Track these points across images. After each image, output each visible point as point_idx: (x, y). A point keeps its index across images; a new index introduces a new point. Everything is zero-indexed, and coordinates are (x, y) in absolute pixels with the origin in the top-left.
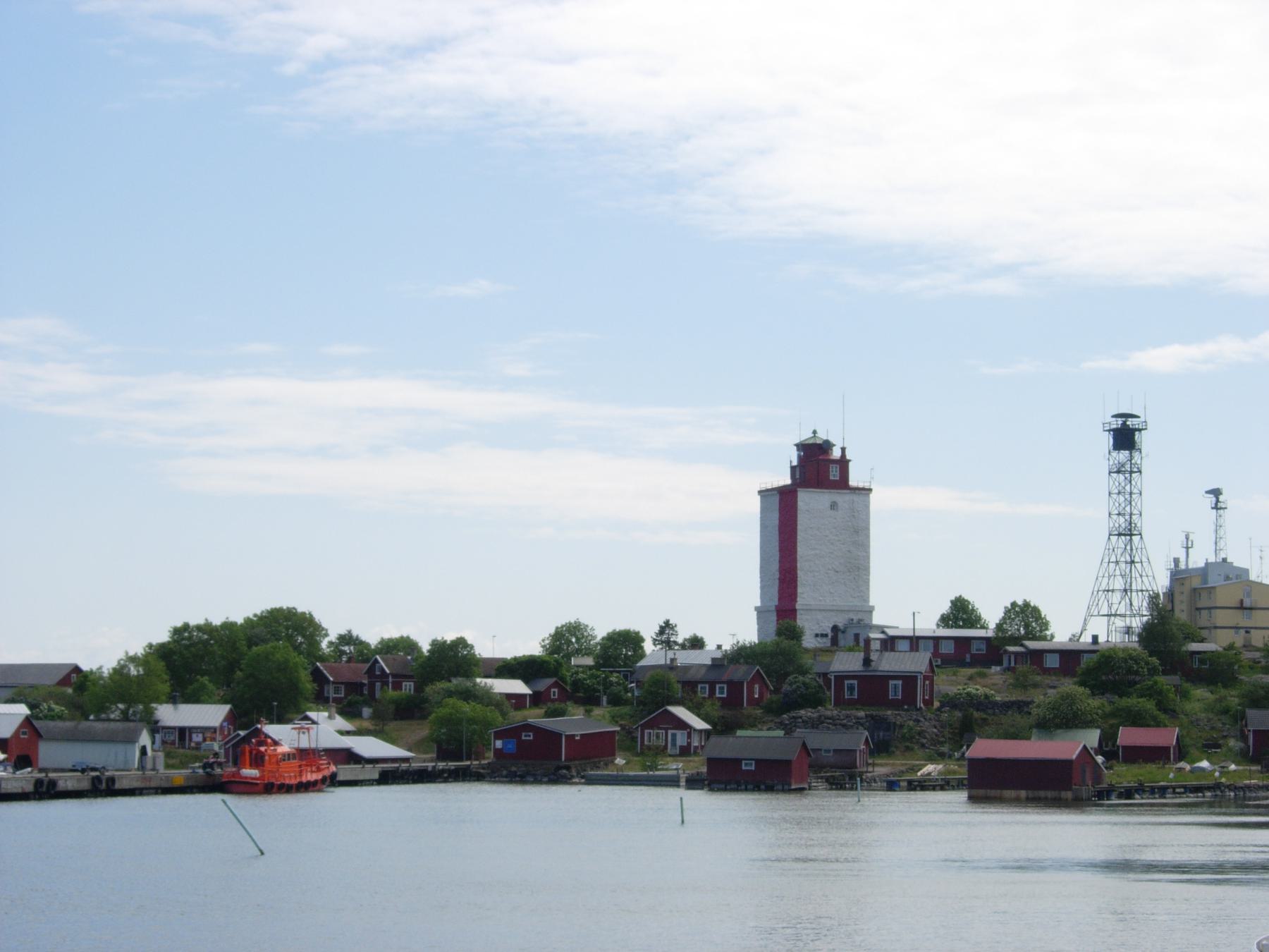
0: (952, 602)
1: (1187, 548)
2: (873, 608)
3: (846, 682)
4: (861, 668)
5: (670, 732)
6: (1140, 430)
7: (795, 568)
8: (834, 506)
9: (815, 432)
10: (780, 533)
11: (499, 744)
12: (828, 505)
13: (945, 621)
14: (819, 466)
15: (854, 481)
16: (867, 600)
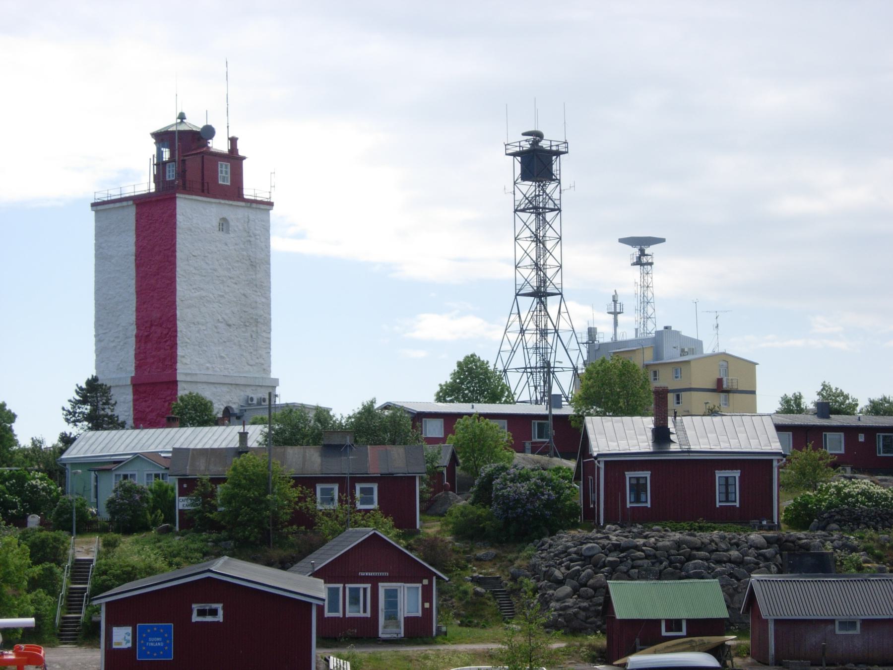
0: (459, 364)
1: (615, 314)
2: (276, 381)
3: (628, 475)
4: (650, 449)
5: (382, 587)
6: (558, 153)
7: (173, 319)
8: (224, 225)
9: (182, 117)
10: (138, 266)
11: (122, 637)
12: (215, 222)
13: (447, 393)
14: (194, 164)
15: (248, 192)
16: (267, 370)
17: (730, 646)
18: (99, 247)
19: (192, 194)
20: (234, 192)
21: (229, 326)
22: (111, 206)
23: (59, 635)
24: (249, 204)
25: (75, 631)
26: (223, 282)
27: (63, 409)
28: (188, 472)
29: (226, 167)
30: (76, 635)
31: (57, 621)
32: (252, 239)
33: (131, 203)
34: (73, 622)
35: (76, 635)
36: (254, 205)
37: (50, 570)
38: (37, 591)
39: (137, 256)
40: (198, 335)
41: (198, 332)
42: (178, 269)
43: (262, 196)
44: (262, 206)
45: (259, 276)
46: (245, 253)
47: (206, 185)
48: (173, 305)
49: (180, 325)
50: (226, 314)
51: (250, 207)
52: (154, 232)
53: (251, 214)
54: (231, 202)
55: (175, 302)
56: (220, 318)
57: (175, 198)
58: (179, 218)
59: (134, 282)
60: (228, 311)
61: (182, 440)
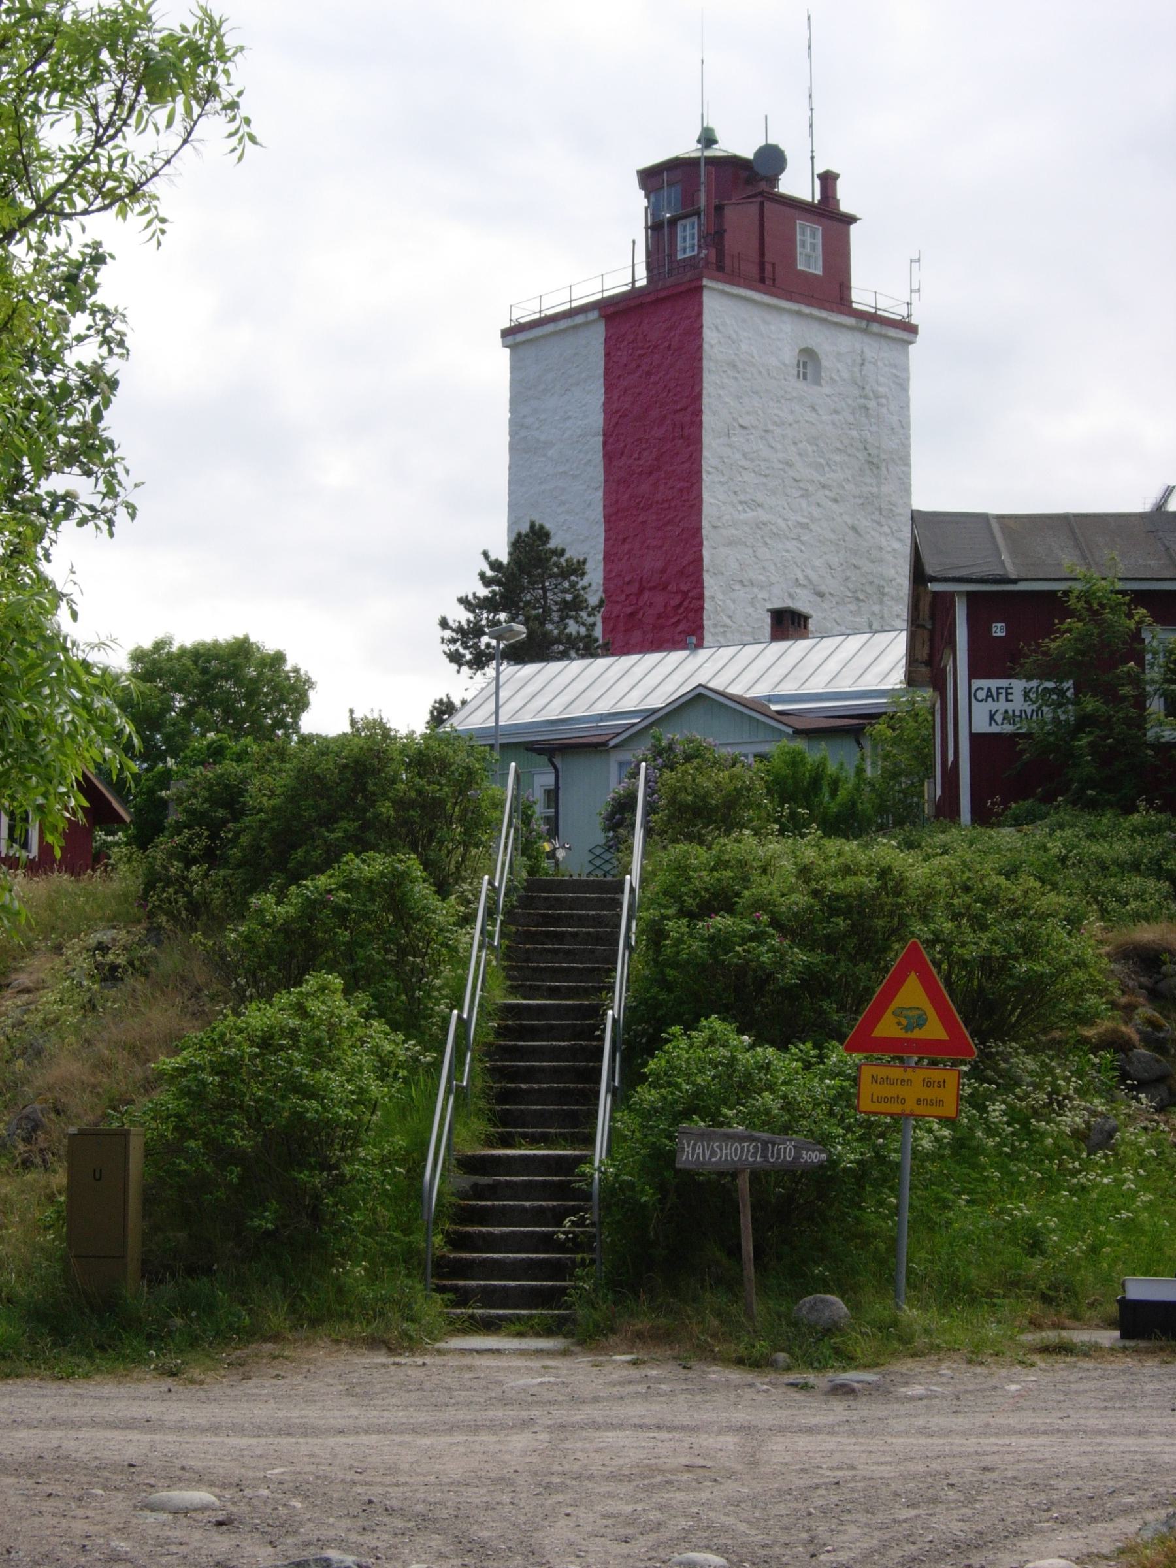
9: (708, 139)
10: (609, 457)
12: (789, 356)
15: (861, 297)
17: (1110, 1324)
18: (517, 426)
19: (739, 285)
20: (830, 291)
21: (821, 595)
22: (550, 328)
23: (445, 1269)
24: (864, 324)
25: (547, 1243)
26: (806, 494)
27: (444, 624)
28: (1012, 573)
29: (814, 236)
30: (557, 1270)
31: (433, 1175)
32: (872, 404)
33: (594, 315)
34: (528, 1191)
35: (557, 1270)
36: (875, 327)
37: (392, 891)
38: (311, 983)
39: (610, 434)
40: (750, 610)
41: (752, 603)
42: (706, 453)
43: (897, 311)
44: (893, 332)
45: (885, 489)
46: (854, 433)
47: (768, 267)
48: (693, 537)
49: (711, 585)
50: (814, 568)
51: (865, 331)
52: (649, 374)
53: (871, 348)
54: (824, 314)
55: (698, 530)
56: (800, 576)
57: (699, 289)
58: (709, 335)
59: (600, 494)
60: (817, 563)
61: (833, 666)
